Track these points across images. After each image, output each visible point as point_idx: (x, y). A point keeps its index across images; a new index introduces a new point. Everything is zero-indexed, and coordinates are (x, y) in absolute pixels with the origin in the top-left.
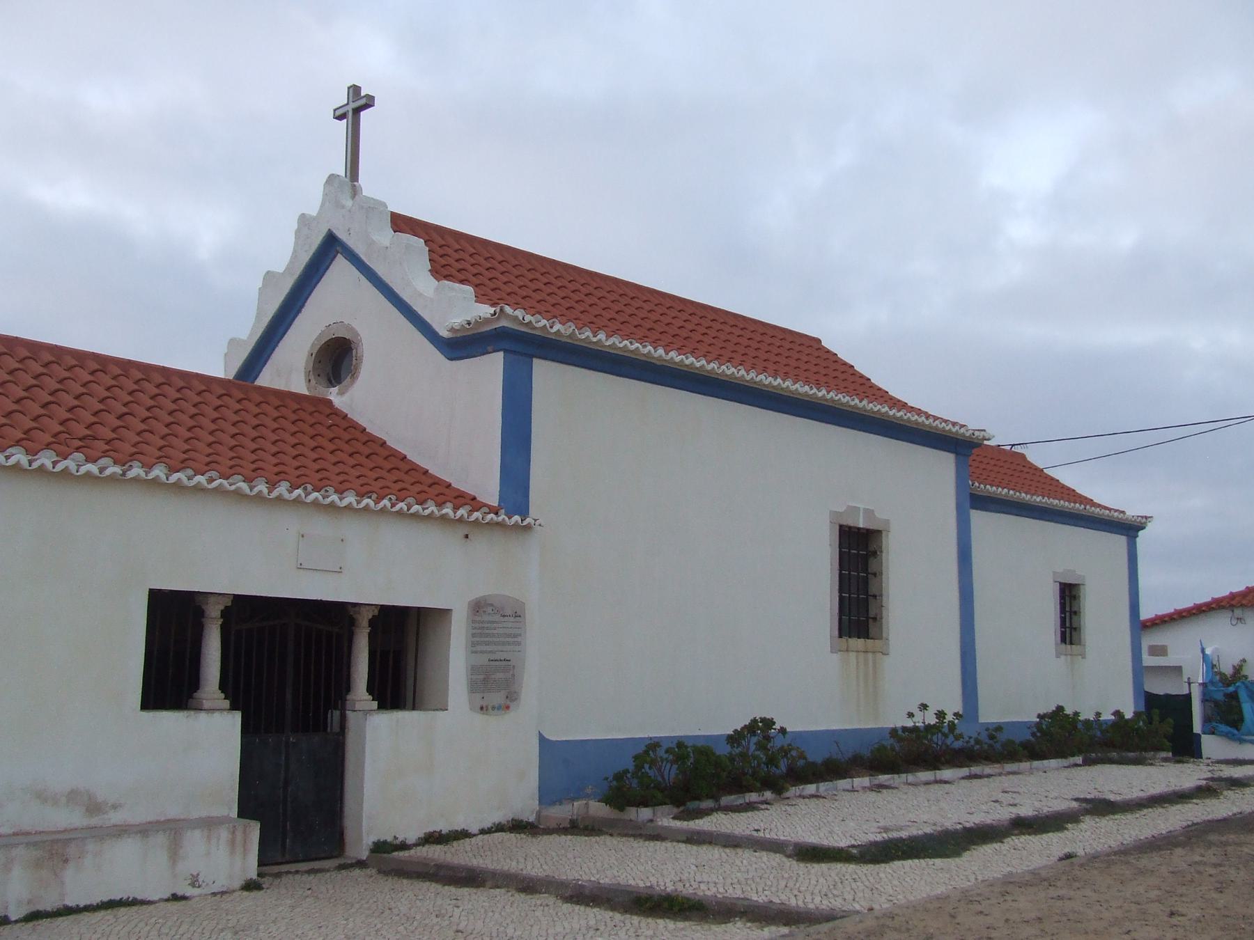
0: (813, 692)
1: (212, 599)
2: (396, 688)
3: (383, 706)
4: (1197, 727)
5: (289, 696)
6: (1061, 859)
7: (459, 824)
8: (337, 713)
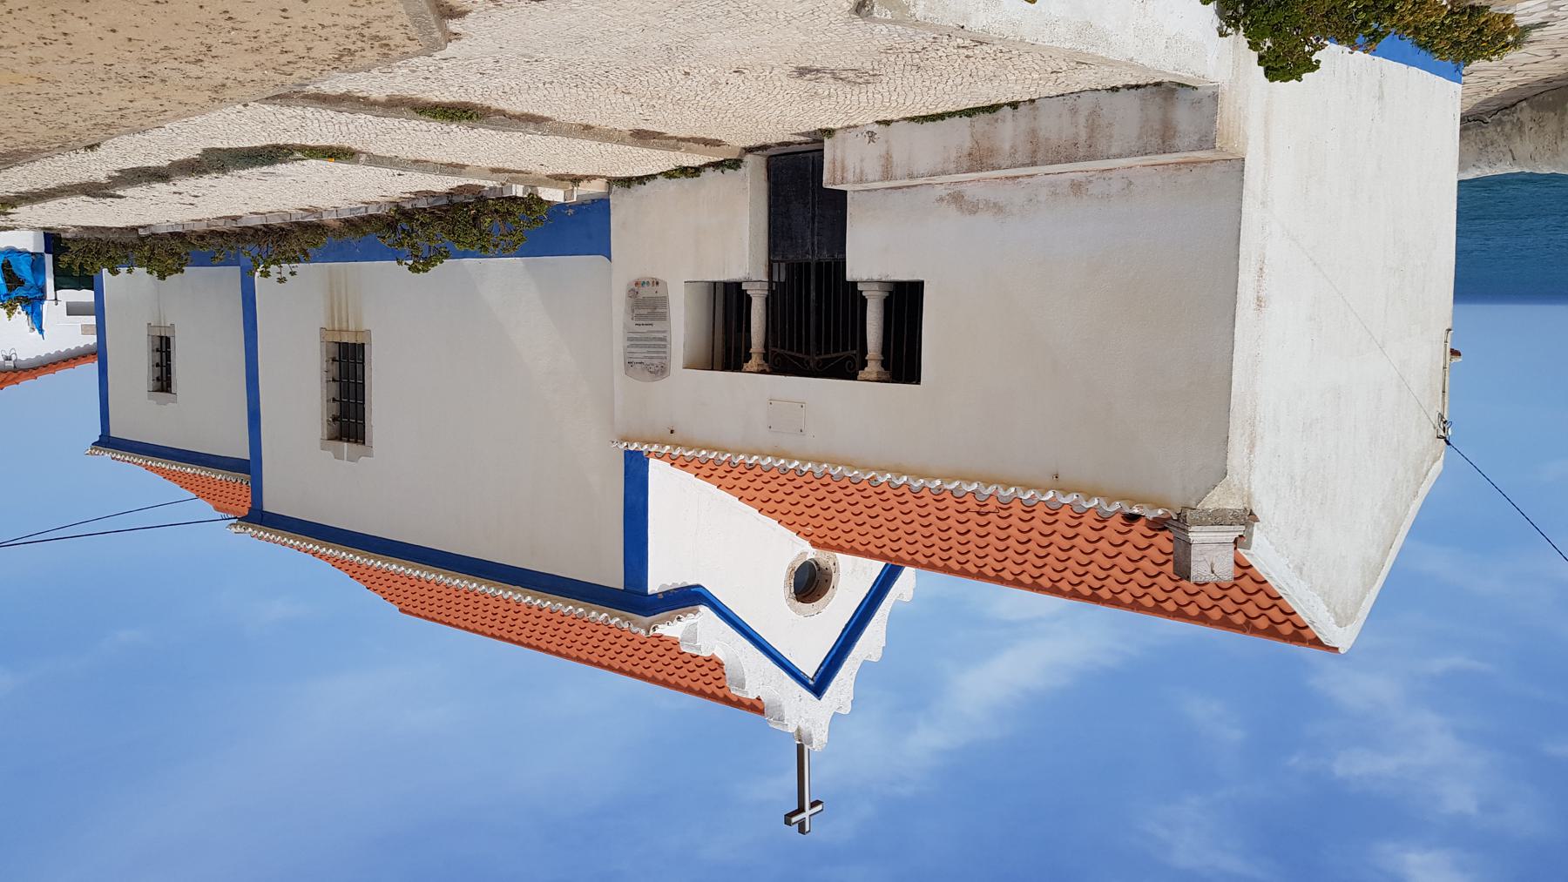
0: (383, 298)
1: (874, 376)
2: (729, 301)
3: (739, 284)
4: (49, 258)
5: (813, 295)
6: (98, 145)
7: (673, 184)
8: (776, 279)
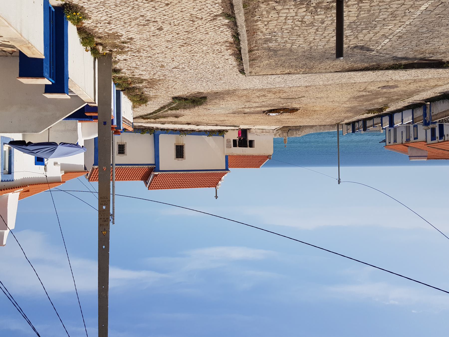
2: (235, 141)
